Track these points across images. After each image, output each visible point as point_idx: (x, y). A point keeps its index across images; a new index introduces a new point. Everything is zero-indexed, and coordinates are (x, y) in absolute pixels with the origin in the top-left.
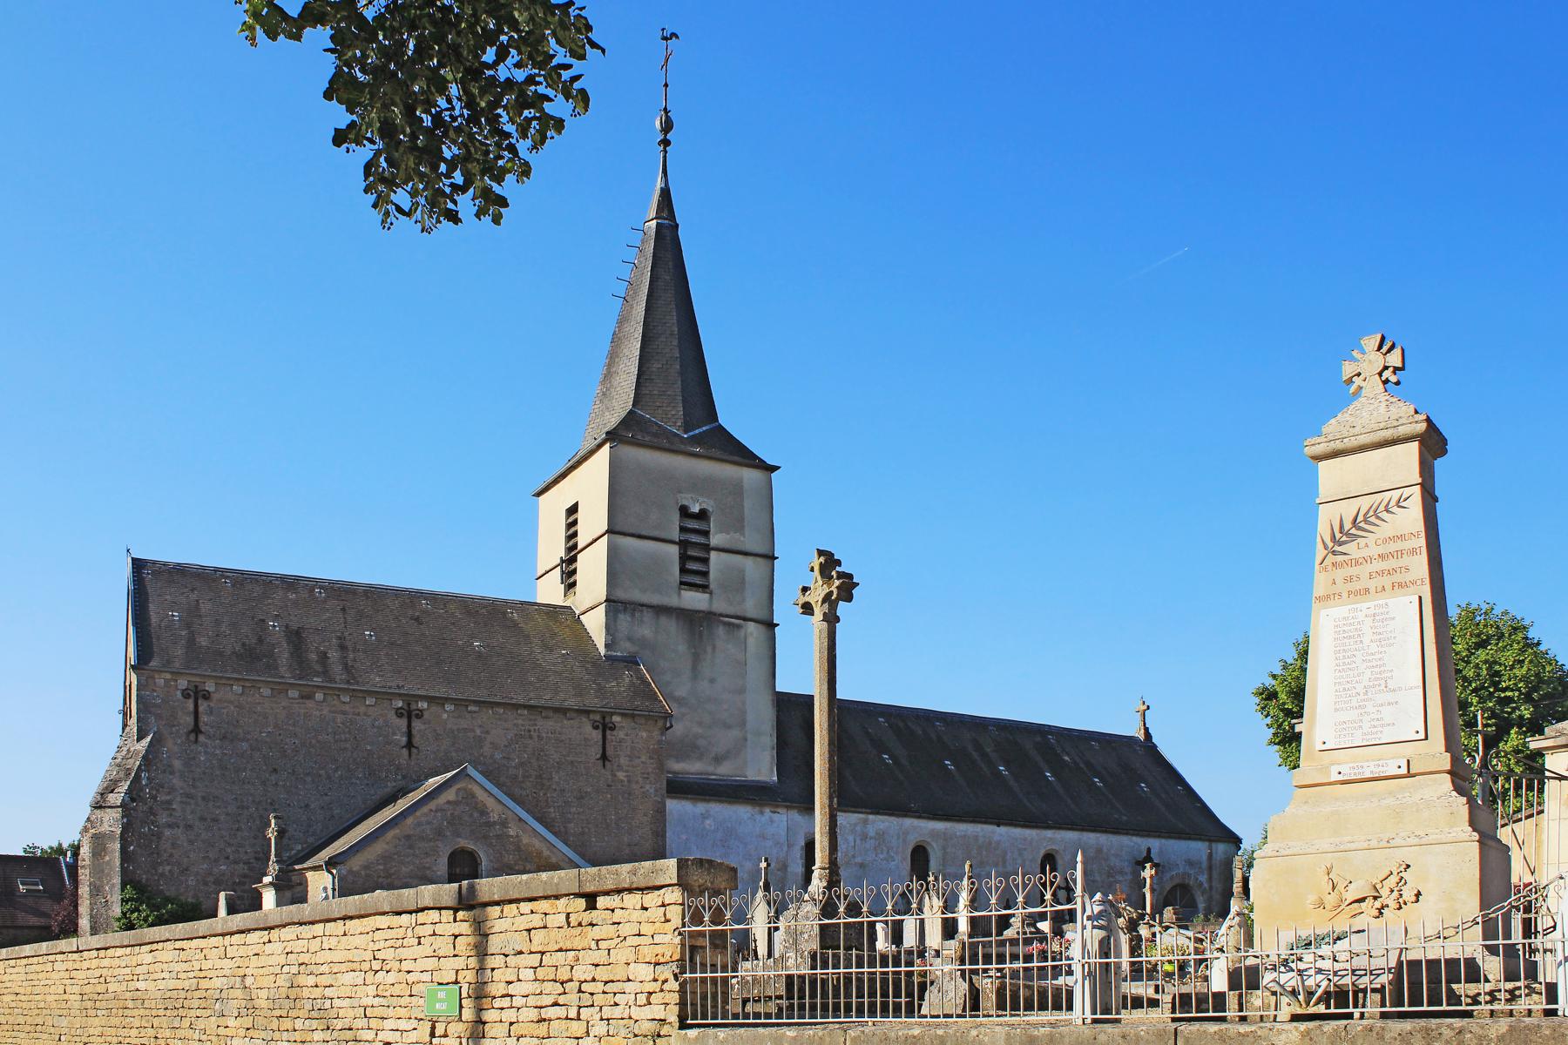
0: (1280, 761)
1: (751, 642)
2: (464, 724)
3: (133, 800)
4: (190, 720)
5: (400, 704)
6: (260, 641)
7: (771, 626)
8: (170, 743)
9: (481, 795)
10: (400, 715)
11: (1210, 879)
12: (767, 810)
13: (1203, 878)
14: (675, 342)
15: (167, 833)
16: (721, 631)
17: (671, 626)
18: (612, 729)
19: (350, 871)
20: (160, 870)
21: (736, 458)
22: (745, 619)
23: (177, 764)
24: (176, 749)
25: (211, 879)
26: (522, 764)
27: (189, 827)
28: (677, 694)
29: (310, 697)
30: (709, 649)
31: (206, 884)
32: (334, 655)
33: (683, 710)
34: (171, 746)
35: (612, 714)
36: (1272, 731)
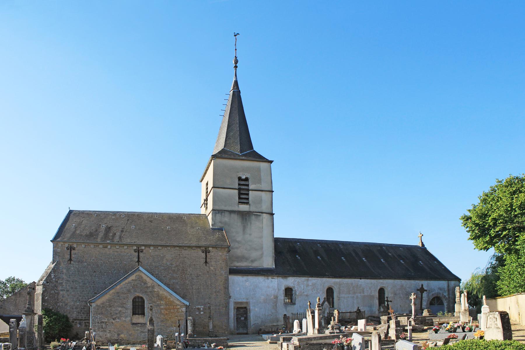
0: (475, 247)
1: (264, 220)
2: (157, 253)
3: (47, 283)
4: (69, 256)
5: (135, 248)
6: (96, 231)
7: (272, 214)
8: (62, 264)
9: (145, 277)
10: (136, 252)
11: (449, 294)
12: (270, 278)
13: (446, 294)
14: (238, 126)
15: (61, 293)
16: (253, 217)
17: (235, 217)
18: (209, 252)
19: (97, 305)
20: (58, 304)
21: (257, 159)
22: (262, 213)
23: (65, 271)
24: (64, 266)
25: (74, 307)
26: (177, 266)
27: (68, 291)
28: (238, 240)
29: (106, 247)
30: (249, 224)
31: (73, 309)
32: (118, 234)
33: (240, 245)
34: (62, 265)
35: (209, 247)
36: (470, 234)
